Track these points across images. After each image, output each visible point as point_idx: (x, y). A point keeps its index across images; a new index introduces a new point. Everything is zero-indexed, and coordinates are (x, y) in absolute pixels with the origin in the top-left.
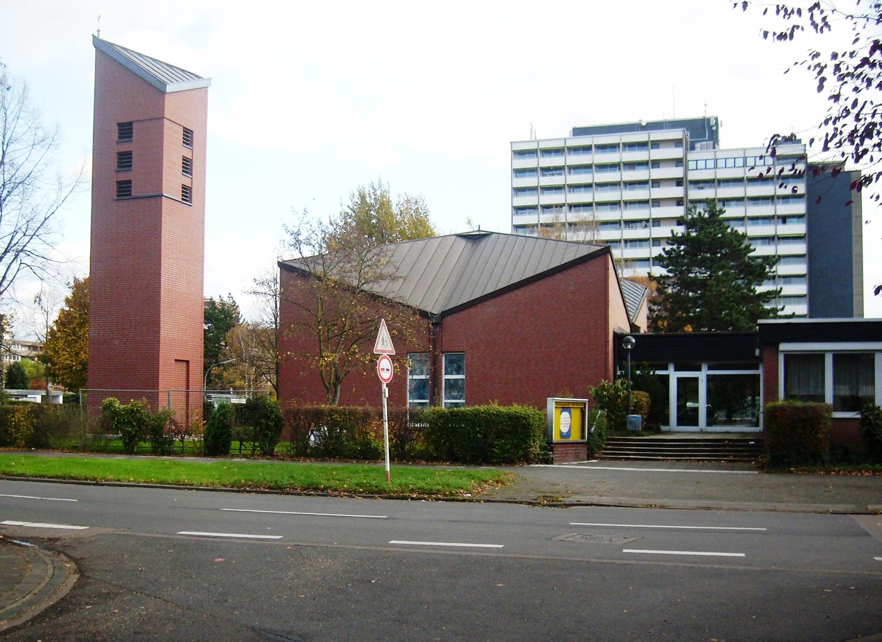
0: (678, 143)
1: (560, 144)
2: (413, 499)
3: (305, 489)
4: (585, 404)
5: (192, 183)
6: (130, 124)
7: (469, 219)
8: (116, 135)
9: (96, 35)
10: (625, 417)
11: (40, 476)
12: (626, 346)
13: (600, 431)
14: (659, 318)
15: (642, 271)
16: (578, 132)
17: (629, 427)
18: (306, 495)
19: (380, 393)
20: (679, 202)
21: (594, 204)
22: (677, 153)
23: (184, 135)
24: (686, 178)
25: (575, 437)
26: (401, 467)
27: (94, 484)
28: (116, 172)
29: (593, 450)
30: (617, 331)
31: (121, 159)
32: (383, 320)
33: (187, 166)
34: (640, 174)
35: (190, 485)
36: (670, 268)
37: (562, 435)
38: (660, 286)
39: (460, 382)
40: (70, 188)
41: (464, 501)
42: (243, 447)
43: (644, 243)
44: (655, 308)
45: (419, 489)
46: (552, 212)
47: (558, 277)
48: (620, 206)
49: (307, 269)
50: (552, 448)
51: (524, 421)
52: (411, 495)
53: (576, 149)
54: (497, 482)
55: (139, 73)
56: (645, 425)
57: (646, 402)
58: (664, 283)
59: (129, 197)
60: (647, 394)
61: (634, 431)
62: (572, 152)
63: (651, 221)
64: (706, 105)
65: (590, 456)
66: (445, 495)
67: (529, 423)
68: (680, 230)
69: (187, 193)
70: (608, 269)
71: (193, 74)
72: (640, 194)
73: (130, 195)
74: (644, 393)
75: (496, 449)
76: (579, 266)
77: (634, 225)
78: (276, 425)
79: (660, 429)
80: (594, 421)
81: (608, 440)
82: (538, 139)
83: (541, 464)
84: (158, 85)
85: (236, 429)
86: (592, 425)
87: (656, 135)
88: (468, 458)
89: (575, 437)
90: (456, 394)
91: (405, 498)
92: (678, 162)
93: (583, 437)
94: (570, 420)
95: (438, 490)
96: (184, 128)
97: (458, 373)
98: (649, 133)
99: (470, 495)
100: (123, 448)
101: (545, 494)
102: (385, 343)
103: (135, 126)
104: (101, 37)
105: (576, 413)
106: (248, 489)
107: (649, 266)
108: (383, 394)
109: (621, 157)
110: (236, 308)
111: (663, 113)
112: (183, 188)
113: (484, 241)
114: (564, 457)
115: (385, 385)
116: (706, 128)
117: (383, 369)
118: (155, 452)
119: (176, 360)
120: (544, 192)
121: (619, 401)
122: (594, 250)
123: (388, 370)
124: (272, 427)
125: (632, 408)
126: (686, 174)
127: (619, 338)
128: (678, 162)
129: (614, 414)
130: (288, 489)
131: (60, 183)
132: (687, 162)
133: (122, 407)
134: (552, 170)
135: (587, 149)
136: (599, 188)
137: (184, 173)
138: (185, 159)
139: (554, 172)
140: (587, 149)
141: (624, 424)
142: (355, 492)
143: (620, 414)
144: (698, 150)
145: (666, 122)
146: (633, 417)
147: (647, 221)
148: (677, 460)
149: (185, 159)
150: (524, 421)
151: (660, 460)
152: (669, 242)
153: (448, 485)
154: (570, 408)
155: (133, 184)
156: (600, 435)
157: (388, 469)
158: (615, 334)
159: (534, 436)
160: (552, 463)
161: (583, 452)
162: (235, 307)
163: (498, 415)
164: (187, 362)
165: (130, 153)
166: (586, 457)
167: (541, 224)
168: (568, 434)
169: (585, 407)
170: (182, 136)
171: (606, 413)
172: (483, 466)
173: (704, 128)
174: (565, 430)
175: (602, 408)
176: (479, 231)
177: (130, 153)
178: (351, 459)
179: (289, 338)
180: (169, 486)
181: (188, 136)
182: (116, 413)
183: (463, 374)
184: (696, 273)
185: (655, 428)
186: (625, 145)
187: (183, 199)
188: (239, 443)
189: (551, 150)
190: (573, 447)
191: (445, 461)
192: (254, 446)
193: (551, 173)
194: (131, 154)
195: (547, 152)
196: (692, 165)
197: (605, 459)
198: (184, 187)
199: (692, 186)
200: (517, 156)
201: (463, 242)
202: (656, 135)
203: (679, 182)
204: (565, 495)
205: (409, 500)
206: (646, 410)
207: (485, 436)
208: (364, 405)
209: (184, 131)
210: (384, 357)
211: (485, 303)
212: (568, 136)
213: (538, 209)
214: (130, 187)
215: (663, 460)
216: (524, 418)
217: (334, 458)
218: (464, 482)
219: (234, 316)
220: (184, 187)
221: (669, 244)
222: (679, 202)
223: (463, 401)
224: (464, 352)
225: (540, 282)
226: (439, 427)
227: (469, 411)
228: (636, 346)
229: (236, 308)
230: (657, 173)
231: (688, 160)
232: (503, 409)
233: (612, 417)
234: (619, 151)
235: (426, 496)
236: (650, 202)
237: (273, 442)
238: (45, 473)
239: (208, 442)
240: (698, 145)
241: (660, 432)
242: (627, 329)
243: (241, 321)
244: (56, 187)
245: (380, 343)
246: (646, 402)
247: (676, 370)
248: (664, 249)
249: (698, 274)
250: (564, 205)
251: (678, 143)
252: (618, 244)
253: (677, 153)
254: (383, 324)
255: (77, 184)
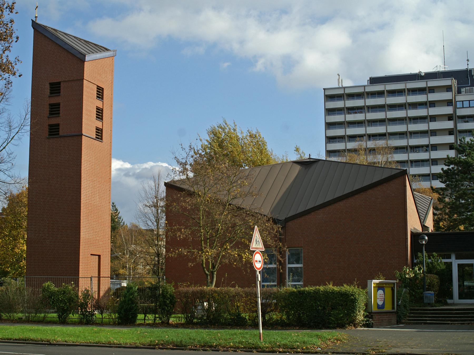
0: (448, 88)
1: (361, 90)
2: (280, 352)
3: (202, 347)
4: (394, 284)
5: (103, 126)
6: (59, 83)
7: (297, 147)
8: (48, 91)
9: (34, 20)
10: (422, 294)
11: (8, 339)
12: (422, 242)
13: (405, 303)
14: (440, 220)
15: (425, 185)
16: (373, 81)
17: (426, 301)
18: (203, 350)
19: (255, 277)
20: (451, 132)
21: (387, 135)
22: (447, 96)
23: (97, 91)
24: (456, 114)
25: (388, 308)
26: (267, 332)
27: (48, 344)
28: (48, 118)
29: (400, 317)
30: (414, 231)
31: (51, 109)
32: (256, 226)
33: (100, 114)
34: (421, 112)
35: (119, 344)
36: (448, 183)
37: (379, 307)
38: (440, 196)
39: (300, 270)
40: (17, 130)
41: (316, 353)
42: (146, 318)
43: (425, 163)
44: (438, 212)
45: (284, 345)
46: (356, 141)
47: (370, 192)
48: (406, 135)
49: (192, 190)
50: (372, 316)
51: (352, 297)
52: (279, 349)
53: (373, 94)
54: (337, 340)
55: (65, 47)
56: (436, 299)
57: (437, 282)
58: (443, 194)
59: (58, 136)
60: (437, 277)
61: (429, 303)
62: (370, 96)
63: (430, 146)
64: (468, 60)
65: (399, 322)
66: (303, 349)
67: (355, 298)
68: (452, 154)
69: (99, 133)
70: (406, 186)
71: (103, 47)
72: (422, 127)
73: (58, 134)
74: (435, 276)
75: (332, 317)
76: (385, 184)
77: (417, 149)
78: (171, 302)
79: (447, 302)
80: (400, 296)
81: (411, 310)
82: (344, 86)
83: (364, 328)
84: (79, 56)
85: (142, 305)
86: (399, 299)
87: (432, 83)
88: (312, 324)
89: (388, 308)
90: (296, 278)
91: (274, 352)
92: (449, 103)
93: (393, 308)
94: (384, 296)
95: (298, 346)
96: (97, 86)
97: (298, 263)
98: (427, 81)
99: (320, 349)
100: (58, 319)
101: (372, 348)
102: (258, 243)
103: (62, 85)
104: (38, 22)
105: (388, 291)
106: (161, 347)
107: (429, 180)
108: (257, 279)
109: (406, 99)
110: (118, 214)
111: (437, 66)
112: (96, 129)
113: (314, 166)
114: (380, 322)
115: (258, 272)
116: (469, 77)
117: (256, 261)
118: (80, 323)
119: (91, 255)
120: (350, 125)
121: (418, 281)
122: (395, 173)
123: (260, 261)
124: (168, 304)
125: (427, 286)
126: (455, 111)
127: (415, 236)
128: (449, 103)
129: (414, 291)
130: (190, 347)
131: (10, 126)
132: (456, 102)
133: (56, 289)
134: (355, 109)
135: (380, 94)
136: (391, 122)
137: (97, 119)
138: (98, 109)
139: (356, 111)
140: (380, 94)
141: (422, 298)
142: (238, 348)
143: (419, 291)
144: (463, 93)
145: (439, 73)
146: (429, 293)
147: (427, 146)
148: (461, 324)
149: (98, 109)
150: (352, 297)
151: (449, 324)
152: (446, 164)
153: (304, 342)
154: (383, 287)
155: (61, 127)
156: (405, 306)
157: (261, 332)
158: (412, 233)
159: (359, 307)
160: (372, 327)
161: (394, 320)
162: (117, 214)
163: (333, 293)
164: (99, 256)
165: (59, 104)
166: (396, 323)
167: (347, 149)
168: (383, 306)
169: (394, 287)
170: (96, 92)
171: (408, 291)
172: (323, 329)
173: (467, 77)
174: (380, 303)
175: (405, 287)
176: (310, 158)
177: (59, 104)
178: (227, 325)
179: (180, 239)
180: (104, 345)
181: (100, 93)
182: (53, 294)
183: (301, 263)
184: (467, 186)
185: (443, 301)
186: (409, 90)
187: (96, 137)
188: (144, 315)
189: (397, 133)
190: (386, 315)
191: (295, 326)
192: (155, 317)
193: (354, 111)
194: (60, 105)
195: (352, 96)
196: (459, 105)
197: (409, 324)
198: (97, 129)
199: (460, 120)
200: (329, 99)
201: (298, 167)
202: (432, 83)
203: (450, 117)
204: (387, 348)
205: (278, 353)
206: (437, 288)
207: (324, 308)
208: (235, 287)
209: (97, 88)
210: (257, 253)
211: (316, 211)
212: (367, 84)
213: (345, 138)
214: (59, 128)
215: (451, 324)
216: (352, 295)
217: (214, 325)
218: (315, 340)
219: (117, 220)
220: (97, 129)
221: (446, 165)
222: (451, 132)
223: (275, 283)
224: (302, 247)
225: (356, 196)
226: (291, 302)
227: (312, 290)
228: (429, 242)
229: (118, 214)
230: (433, 111)
231: (456, 101)
232: (336, 289)
233: (412, 294)
234: (405, 95)
235: (289, 350)
236: (429, 132)
237: (169, 314)
238: (10, 337)
239: (121, 315)
240: (463, 90)
241: (447, 304)
242: (420, 229)
243: (122, 224)
244: (7, 129)
245: (255, 243)
246: (437, 282)
247: (457, 258)
248: (442, 169)
249: (468, 187)
250: (365, 135)
251: (448, 88)
252: (406, 164)
253: (447, 96)
254: (256, 229)
255: (22, 127)
